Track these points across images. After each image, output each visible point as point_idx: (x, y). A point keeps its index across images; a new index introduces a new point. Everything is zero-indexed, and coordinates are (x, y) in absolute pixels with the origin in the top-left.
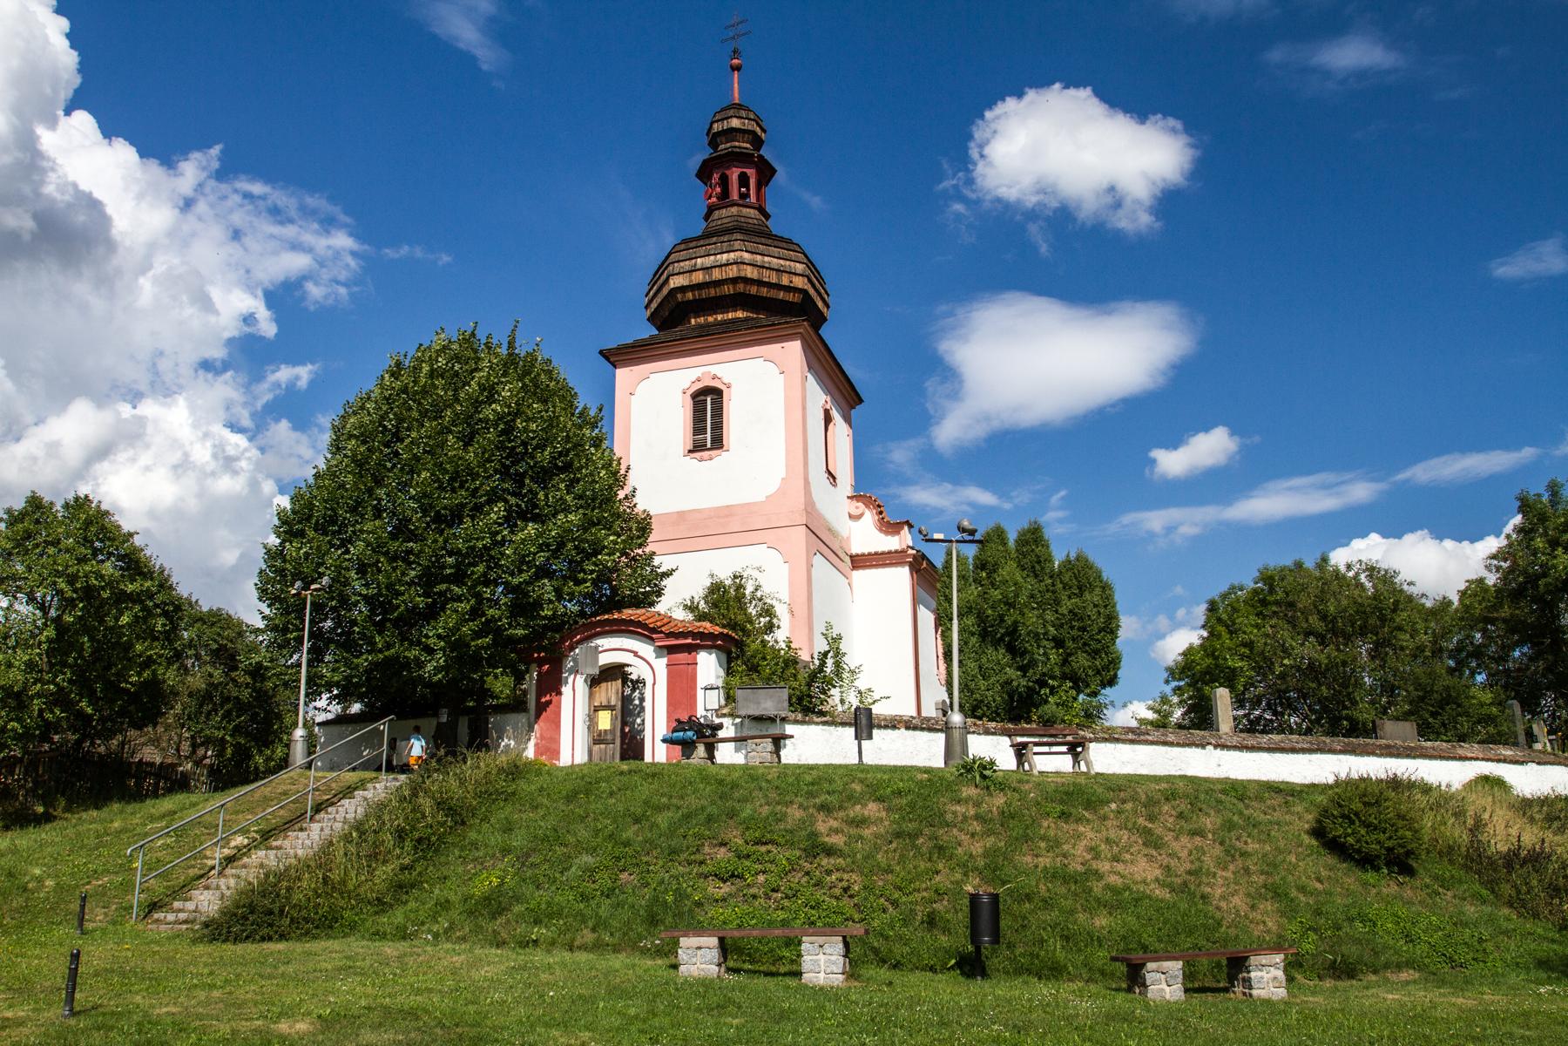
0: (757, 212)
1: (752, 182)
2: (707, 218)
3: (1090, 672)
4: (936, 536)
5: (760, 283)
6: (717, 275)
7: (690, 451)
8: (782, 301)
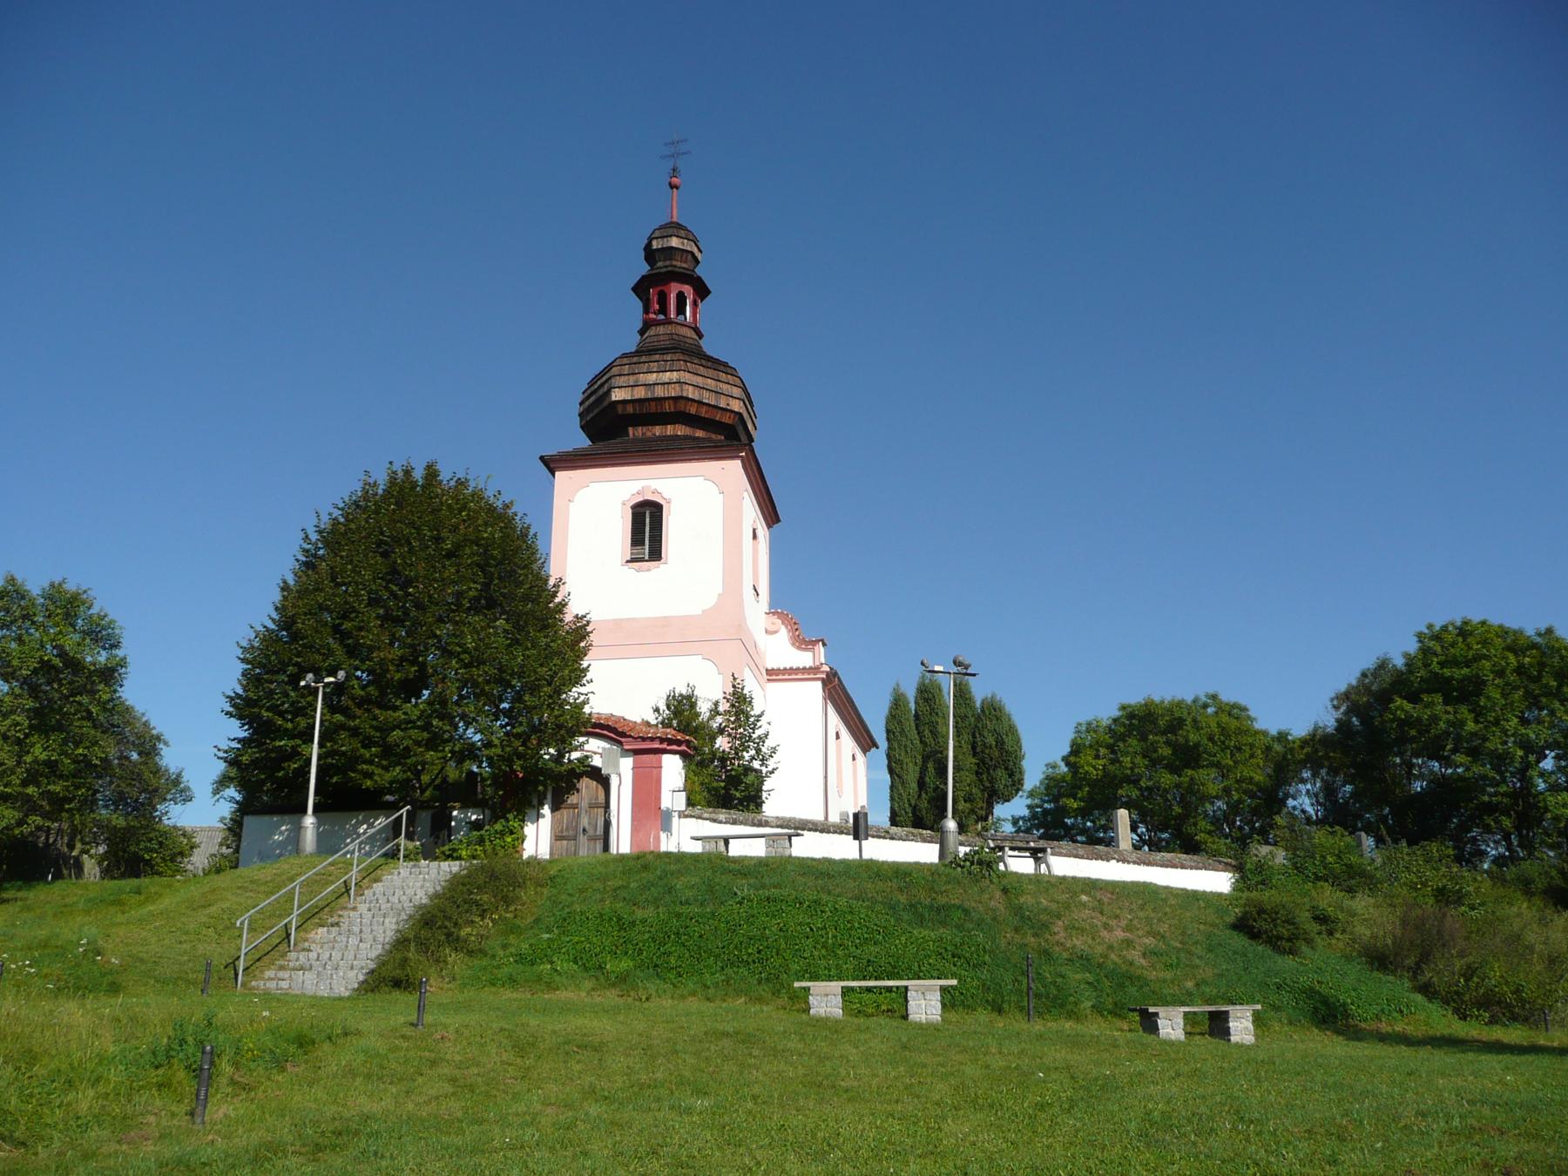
2: (642, 332)
4: (937, 668)
7: (628, 562)
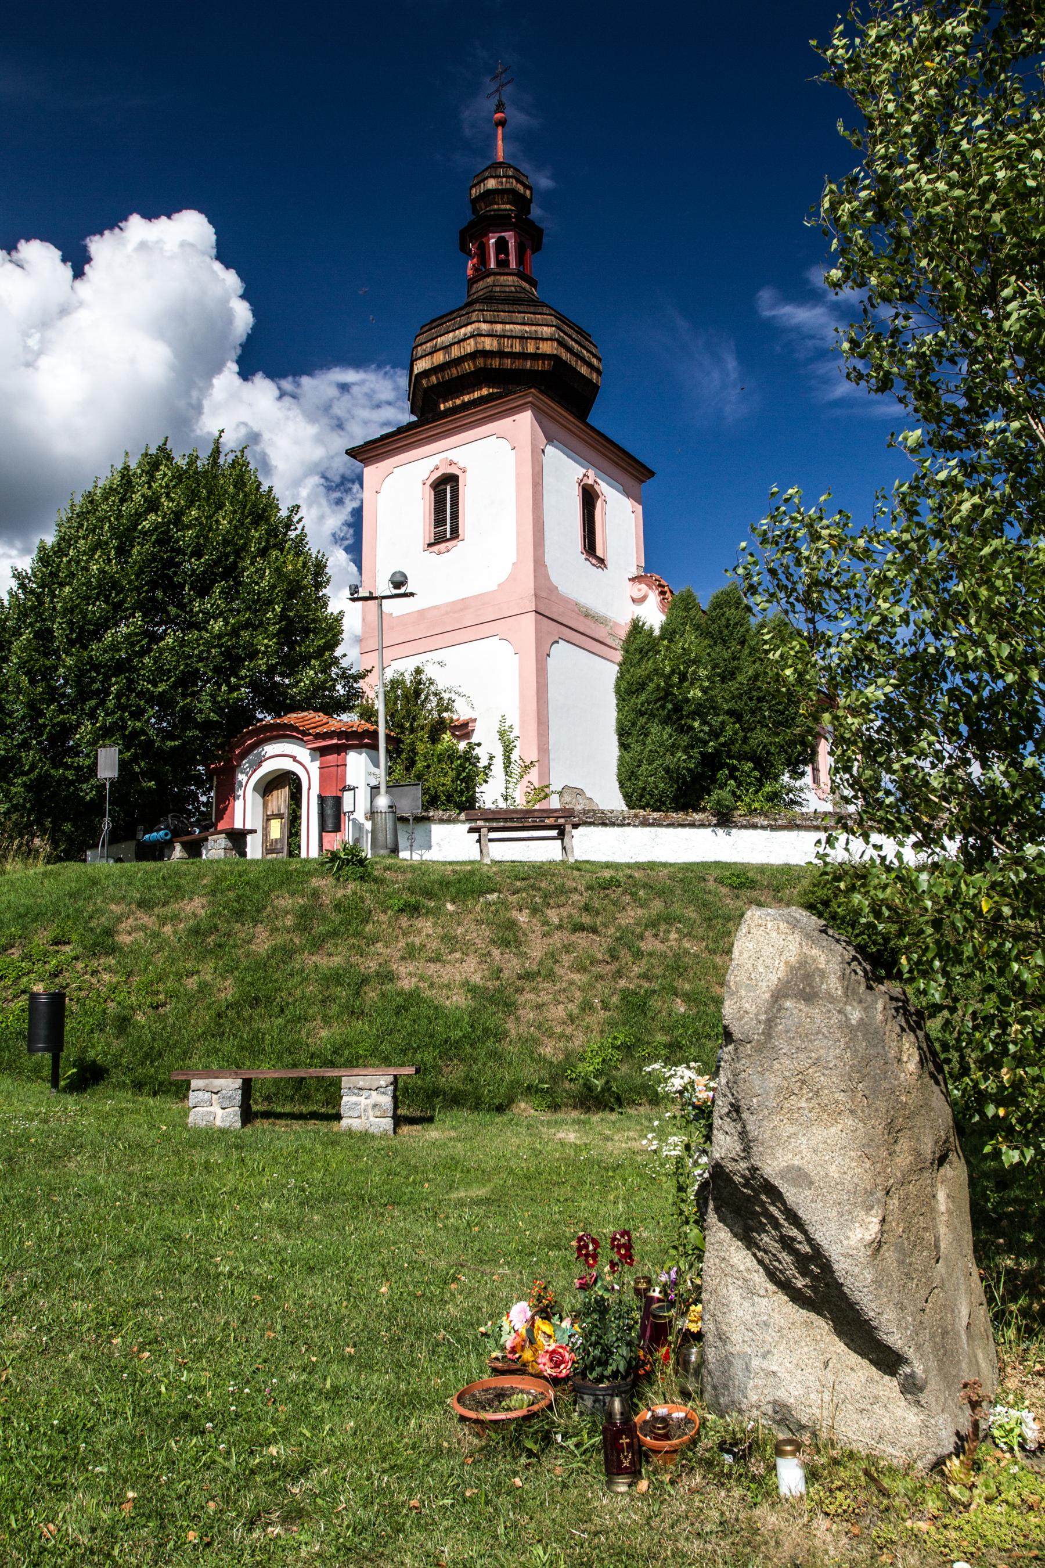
0: (515, 278)
1: (512, 244)
3: (773, 749)
5: (501, 354)
6: (456, 352)
7: (430, 545)
8: (530, 371)
